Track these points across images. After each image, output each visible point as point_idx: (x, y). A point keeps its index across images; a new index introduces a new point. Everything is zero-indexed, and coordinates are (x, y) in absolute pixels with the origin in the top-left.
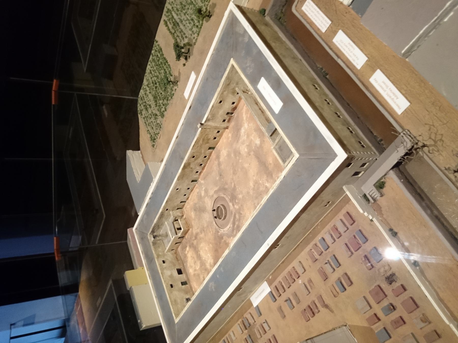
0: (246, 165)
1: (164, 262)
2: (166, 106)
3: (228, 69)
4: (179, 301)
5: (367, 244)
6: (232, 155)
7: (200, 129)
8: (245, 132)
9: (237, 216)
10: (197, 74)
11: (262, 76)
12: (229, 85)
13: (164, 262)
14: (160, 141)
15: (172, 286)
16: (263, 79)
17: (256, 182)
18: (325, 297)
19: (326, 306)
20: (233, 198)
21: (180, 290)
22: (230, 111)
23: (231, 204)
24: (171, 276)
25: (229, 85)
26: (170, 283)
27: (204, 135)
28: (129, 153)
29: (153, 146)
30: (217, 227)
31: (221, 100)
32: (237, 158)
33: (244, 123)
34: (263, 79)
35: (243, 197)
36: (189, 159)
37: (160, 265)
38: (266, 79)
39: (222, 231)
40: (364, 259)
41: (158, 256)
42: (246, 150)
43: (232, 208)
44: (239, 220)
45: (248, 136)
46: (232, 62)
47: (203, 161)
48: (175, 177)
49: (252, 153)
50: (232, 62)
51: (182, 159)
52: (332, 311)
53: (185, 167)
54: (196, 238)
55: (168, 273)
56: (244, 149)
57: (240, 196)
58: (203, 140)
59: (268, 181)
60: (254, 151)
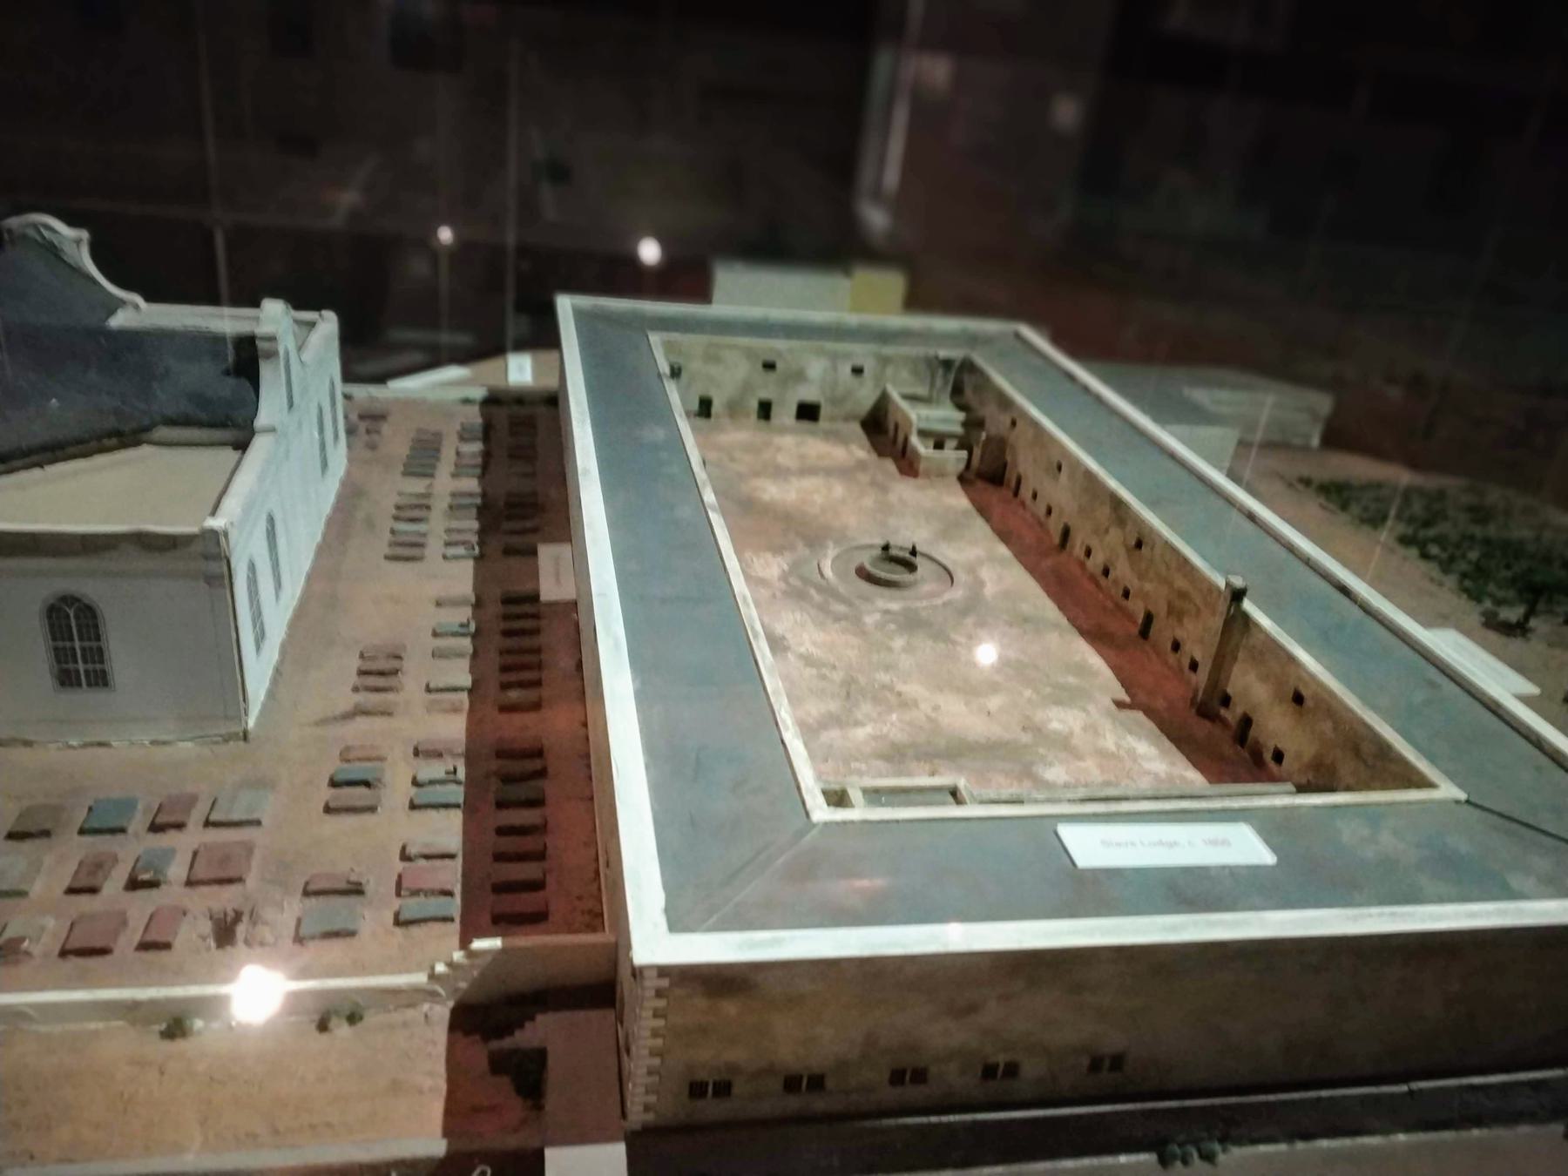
0: (994, 702)
1: (858, 371)
2: (1441, 563)
3: (1423, 765)
4: (714, 370)
5: (389, 918)
6: (1072, 680)
7: (1222, 583)
8: (1132, 754)
9: (840, 608)
10: (1526, 700)
11: (1279, 859)
12: (1357, 752)
13: (858, 371)
14: (1313, 506)
15: (769, 366)
16: (1267, 857)
17: (905, 703)
18: (378, 723)
19: (348, 716)
20: (911, 623)
21: (747, 387)
22: (1253, 733)
23: (895, 606)
24: (800, 376)
25: (1357, 752)
26: (779, 365)
27: (1198, 601)
28: (1324, 403)
29: (1307, 482)
30: (854, 544)
31: (1309, 703)
32: (1048, 690)
33: (1173, 764)
34: (1267, 857)
35: (890, 649)
36: (1139, 522)
37: (847, 356)
38: (1255, 870)
39: (832, 552)
40: (353, 878)
41: (884, 361)
42: (1055, 725)
43: (881, 604)
44: (823, 609)
45: (1102, 754)
46: (1448, 791)
47: (1115, 582)
48: (1102, 464)
49: (1026, 738)
50: (1448, 791)
51: (1153, 505)
52: (323, 722)
53: (1117, 504)
54: (873, 483)
55: (816, 368)
56: (1061, 721)
57: (898, 643)
58: (1183, 595)
59: (875, 738)
60: (1026, 746)
